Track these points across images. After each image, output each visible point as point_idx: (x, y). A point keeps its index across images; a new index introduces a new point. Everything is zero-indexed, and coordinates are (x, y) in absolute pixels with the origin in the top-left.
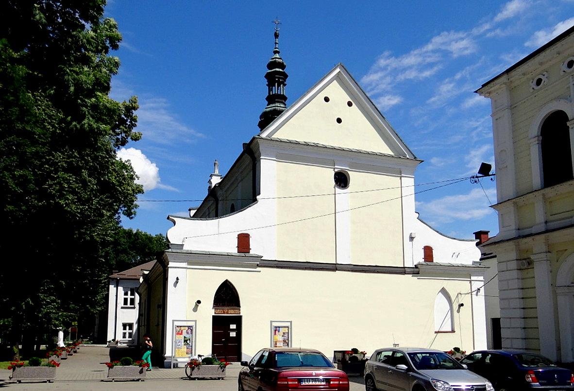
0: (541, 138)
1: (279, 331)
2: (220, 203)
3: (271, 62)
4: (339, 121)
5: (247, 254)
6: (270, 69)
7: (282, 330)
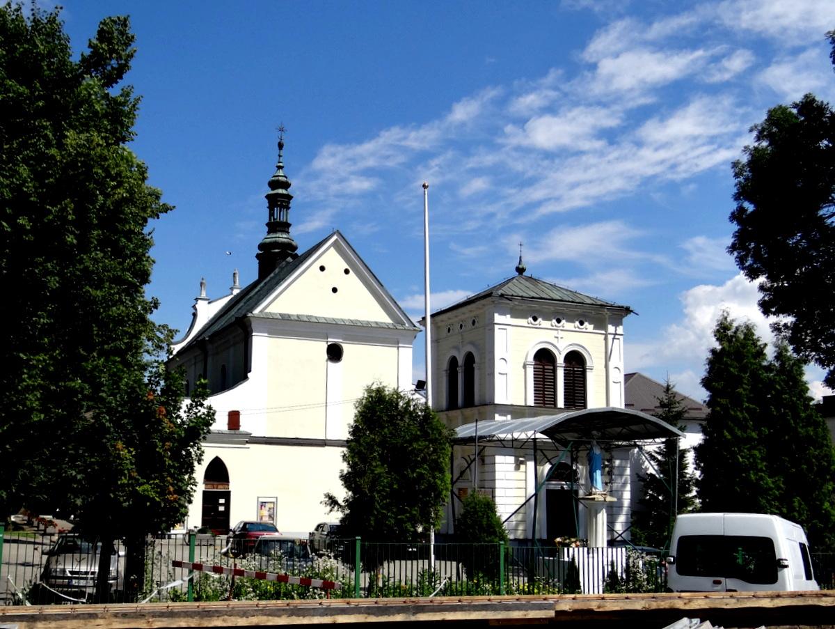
0: (448, 372)
1: (265, 506)
2: (210, 360)
3: (273, 181)
4: (335, 290)
5: (237, 432)
6: (273, 189)
7: (268, 506)
